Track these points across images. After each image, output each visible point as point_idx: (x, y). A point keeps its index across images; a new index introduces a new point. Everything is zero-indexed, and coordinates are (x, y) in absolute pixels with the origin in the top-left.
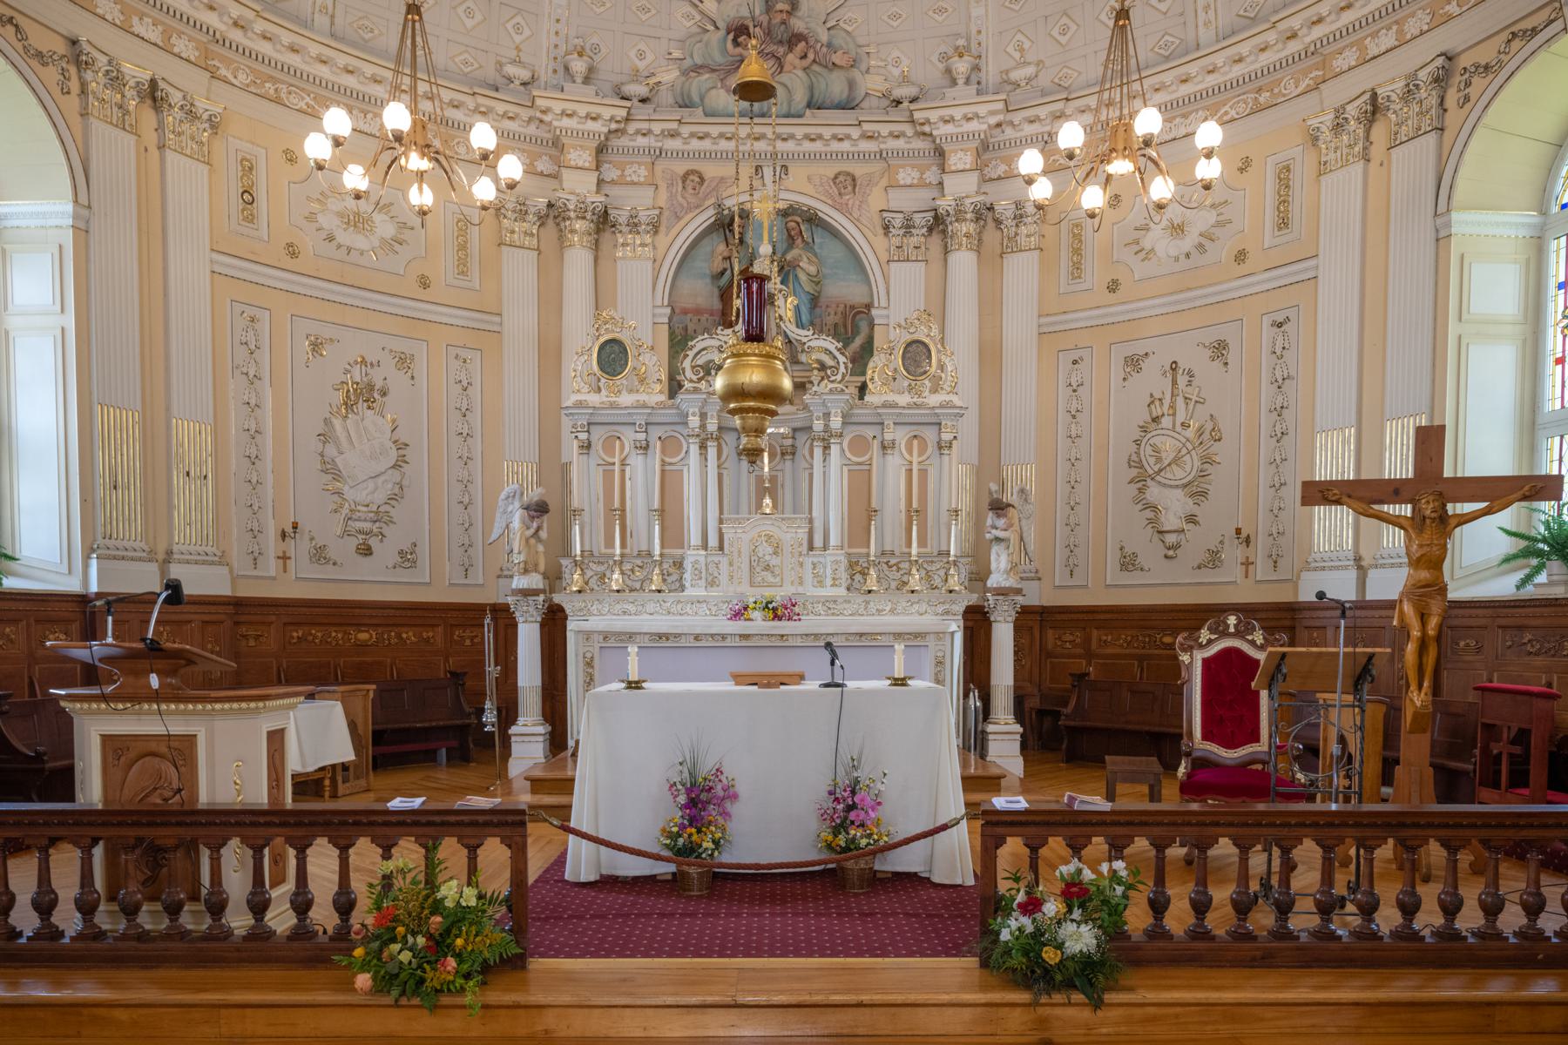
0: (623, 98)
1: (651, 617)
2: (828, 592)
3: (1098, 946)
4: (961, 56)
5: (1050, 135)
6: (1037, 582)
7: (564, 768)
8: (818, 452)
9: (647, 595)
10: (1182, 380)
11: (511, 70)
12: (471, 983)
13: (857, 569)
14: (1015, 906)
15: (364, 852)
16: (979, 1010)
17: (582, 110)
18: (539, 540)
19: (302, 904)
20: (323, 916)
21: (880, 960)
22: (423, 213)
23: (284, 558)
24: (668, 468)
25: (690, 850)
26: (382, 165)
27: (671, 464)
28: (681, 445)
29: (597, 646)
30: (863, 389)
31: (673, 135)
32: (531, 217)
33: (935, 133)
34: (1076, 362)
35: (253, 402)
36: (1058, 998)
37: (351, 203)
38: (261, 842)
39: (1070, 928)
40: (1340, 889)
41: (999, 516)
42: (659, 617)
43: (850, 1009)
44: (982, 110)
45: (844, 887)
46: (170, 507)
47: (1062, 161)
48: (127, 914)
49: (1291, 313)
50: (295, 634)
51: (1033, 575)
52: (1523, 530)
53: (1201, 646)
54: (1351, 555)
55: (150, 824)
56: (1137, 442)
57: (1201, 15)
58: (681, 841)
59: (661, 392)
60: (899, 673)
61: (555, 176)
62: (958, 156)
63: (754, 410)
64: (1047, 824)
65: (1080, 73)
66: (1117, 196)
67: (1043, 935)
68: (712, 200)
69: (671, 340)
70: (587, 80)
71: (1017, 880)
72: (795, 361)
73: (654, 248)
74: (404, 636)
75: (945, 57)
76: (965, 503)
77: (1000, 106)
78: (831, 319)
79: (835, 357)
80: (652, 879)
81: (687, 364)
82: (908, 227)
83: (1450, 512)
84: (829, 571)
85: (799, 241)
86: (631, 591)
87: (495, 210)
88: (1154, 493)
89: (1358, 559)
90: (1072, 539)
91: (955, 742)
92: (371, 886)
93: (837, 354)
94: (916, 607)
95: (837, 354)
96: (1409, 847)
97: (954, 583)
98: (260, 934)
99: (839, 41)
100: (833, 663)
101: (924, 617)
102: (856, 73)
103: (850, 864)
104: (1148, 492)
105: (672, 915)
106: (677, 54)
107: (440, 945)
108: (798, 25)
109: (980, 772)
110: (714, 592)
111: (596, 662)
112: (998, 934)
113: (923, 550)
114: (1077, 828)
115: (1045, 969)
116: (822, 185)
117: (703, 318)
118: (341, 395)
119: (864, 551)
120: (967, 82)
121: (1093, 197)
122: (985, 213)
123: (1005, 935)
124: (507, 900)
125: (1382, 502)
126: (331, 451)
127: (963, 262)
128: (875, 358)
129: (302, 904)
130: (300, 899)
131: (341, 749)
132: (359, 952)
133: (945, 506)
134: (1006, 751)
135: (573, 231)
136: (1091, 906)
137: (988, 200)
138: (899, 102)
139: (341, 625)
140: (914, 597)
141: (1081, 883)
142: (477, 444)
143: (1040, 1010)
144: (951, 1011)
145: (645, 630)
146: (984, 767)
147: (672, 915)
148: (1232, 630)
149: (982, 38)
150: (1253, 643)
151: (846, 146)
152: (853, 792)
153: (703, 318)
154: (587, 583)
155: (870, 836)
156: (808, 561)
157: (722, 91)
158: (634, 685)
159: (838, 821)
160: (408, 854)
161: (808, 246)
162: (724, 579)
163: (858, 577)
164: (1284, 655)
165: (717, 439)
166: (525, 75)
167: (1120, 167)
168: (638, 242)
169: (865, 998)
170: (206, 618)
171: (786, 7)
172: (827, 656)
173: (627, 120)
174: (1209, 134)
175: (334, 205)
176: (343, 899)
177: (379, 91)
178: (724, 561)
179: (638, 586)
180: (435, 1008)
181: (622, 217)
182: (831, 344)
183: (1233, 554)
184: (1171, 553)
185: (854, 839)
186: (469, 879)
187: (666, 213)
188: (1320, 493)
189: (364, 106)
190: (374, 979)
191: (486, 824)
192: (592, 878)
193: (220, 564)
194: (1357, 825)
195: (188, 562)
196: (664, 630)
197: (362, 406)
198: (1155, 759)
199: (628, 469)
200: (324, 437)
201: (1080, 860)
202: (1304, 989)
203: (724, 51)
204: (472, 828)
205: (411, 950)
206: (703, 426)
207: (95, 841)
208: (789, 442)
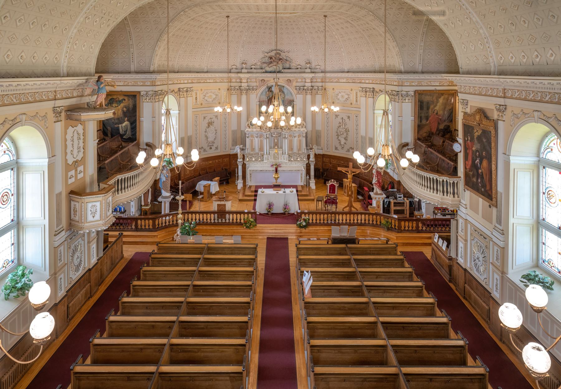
2: (286, 161)
9: (258, 162)
10: (344, 121)
25: (269, 212)
107: (251, 225)
108: (281, 57)
135: (243, 93)
162: (270, 159)
178: (270, 156)
200: (205, 132)
203: (268, 60)
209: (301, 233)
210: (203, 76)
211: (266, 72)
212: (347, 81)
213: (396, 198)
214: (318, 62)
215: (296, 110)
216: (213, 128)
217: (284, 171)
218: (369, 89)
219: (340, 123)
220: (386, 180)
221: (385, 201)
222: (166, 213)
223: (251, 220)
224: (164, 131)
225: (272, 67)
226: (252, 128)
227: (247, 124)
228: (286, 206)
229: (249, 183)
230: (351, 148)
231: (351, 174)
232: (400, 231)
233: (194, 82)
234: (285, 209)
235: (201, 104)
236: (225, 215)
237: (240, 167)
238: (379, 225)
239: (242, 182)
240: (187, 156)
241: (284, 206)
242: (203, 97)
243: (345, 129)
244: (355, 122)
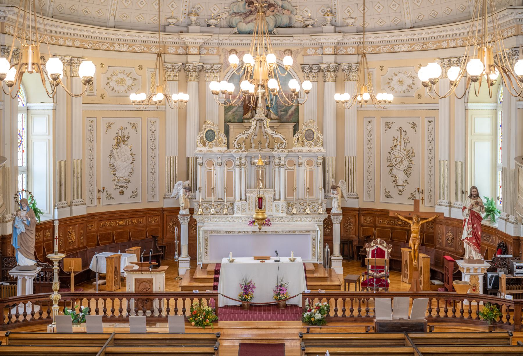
2: (280, 214)
6: (357, 200)
10: (403, 134)
13: (289, 205)
23: (99, 199)
25: (245, 300)
27: (229, 170)
29: (209, 235)
39: (317, 314)
42: (226, 223)
50: (102, 224)
51: (356, 196)
53: (371, 247)
57: (406, 15)
58: (243, 298)
62: (328, 49)
65: (369, 24)
74: (133, 221)
84: (280, 208)
90: (369, 185)
94: (308, 219)
103: (280, 303)
107: (205, 318)
123: (305, 316)
135: (192, 76)
139: (114, 219)
148: (379, 243)
149: (336, 6)
150: (384, 246)
152: (281, 287)
156: (274, 204)
157: (244, 23)
160: (196, 301)
162: (247, 209)
163: (290, 208)
168: (213, 76)
170: (80, 222)
178: (247, 204)
179: (219, 211)
184: (400, 193)
192: (223, 306)
196: (229, 230)
197: (121, 144)
200: (111, 156)
203: (244, 8)
210: (106, 36)
211: (240, 33)
212: (410, 49)
213: (511, 272)
214: (349, 11)
215: (304, 115)
216: (128, 149)
217: (276, 232)
218: (456, 59)
219: (395, 139)
220: (490, 246)
221: (489, 275)
222: (27, 293)
223: (206, 308)
224: (24, 146)
225: (251, 21)
226: (209, 145)
227: (198, 138)
228: (280, 289)
229: (201, 260)
230: (418, 189)
231: (418, 222)
232: (517, 327)
233: (86, 45)
234: (278, 294)
235: (102, 96)
236: (152, 301)
237: (184, 228)
238: (476, 319)
239: (189, 259)
240: (71, 203)
241: (276, 289)
242: (107, 81)
243: (405, 152)
244: (427, 133)
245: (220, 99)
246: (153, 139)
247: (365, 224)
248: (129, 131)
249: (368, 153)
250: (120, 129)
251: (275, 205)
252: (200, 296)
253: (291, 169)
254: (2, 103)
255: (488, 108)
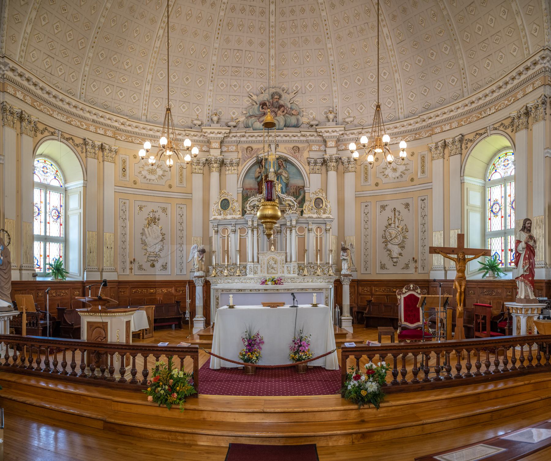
0: (228, 126)
1: (236, 284)
2: (292, 275)
3: (378, 389)
4: (331, 113)
5: (358, 138)
6: (356, 272)
7: (209, 331)
8: (288, 232)
9: (235, 277)
10: (397, 214)
11: (195, 122)
12: (181, 402)
13: (301, 268)
14: (352, 378)
15: (151, 358)
16: (341, 412)
17: (216, 131)
18: (203, 261)
19: (134, 373)
20: (140, 377)
21: (310, 396)
22: (170, 167)
23: (131, 269)
24: (242, 237)
25: (248, 360)
26: (159, 155)
27: (242, 236)
28: (246, 230)
29: (220, 293)
30: (302, 212)
31: (243, 136)
32: (201, 164)
33: (323, 135)
34: (366, 206)
35: (124, 226)
36: (366, 406)
37: (151, 167)
38: (123, 354)
39: (369, 384)
40: (442, 364)
41: (344, 252)
43: (300, 414)
44: (338, 129)
45: (298, 371)
46: (103, 257)
47: (361, 146)
48: (92, 371)
49: (426, 197)
52: (483, 262)
53: (403, 294)
54: (443, 267)
55: (98, 347)
56: (385, 231)
58: (246, 357)
59: (240, 214)
60: (315, 303)
61: (208, 151)
63: (269, 222)
64: (362, 351)
66: (377, 158)
67: (361, 386)
68: (255, 155)
69: (243, 198)
70: (218, 122)
71: (353, 369)
72: (281, 203)
73: (238, 170)
75: (326, 113)
76: (334, 248)
77: (343, 129)
78: (292, 191)
79: (293, 203)
80: (237, 369)
81: (248, 205)
82: (316, 163)
83: (466, 258)
84: (292, 269)
85: (282, 167)
86: (230, 276)
87: (191, 163)
88: (390, 246)
89: (445, 268)
91: (332, 322)
92: (153, 369)
93: (294, 202)
94: (319, 280)
95: (294, 202)
96: (458, 352)
97: (331, 272)
98: (122, 381)
99: (294, 107)
100: (294, 300)
101: (322, 283)
102: (299, 117)
104: (388, 246)
105: (243, 381)
106: (245, 112)
107: (172, 389)
108: (281, 102)
109: (340, 332)
110: (256, 276)
111: (219, 299)
112: (347, 387)
113: (321, 262)
114: (370, 351)
115: (362, 397)
116: (289, 150)
117: (252, 191)
118: (147, 222)
119: (303, 262)
120: (333, 121)
121: (371, 158)
122: (339, 160)
123: (349, 387)
124: (192, 375)
125: (450, 254)
126: (144, 237)
127: (332, 174)
128: (306, 203)
129: (134, 373)
130: (133, 371)
131: (145, 325)
132: (149, 389)
133: (328, 249)
134: (347, 326)
135: (213, 167)
136: (375, 376)
137: (340, 156)
138: (312, 126)
140: (319, 277)
141: (372, 369)
142: (184, 233)
143: (361, 411)
144: (333, 413)
145: (235, 288)
146: (341, 331)
147: (243, 381)
148: (412, 289)
149: (337, 108)
150: (417, 292)
151: (296, 138)
152: (301, 341)
153: (252, 191)
154: (217, 274)
155: (306, 355)
156: (285, 266)
158: (231, 307)
159: (296, 350)
160: (163, 359)
161: (285, 168)
162: (259, 271)
164: (425, 297)
165: (257, 228)
166: (199, 123)
167: (378, 150)
168: (233, 169)
169: (305, 409)
171: (278, 97)
172: (292, 297)
173: (229, 133)
174: (403, 144)
175: (146, 168)
176: (145, 372)
177: (159, 134)
178: (259, 266)
179: (232, 274)
180: (171, 408)
181: (228, 162)
182: (292, 199)
183: (412, 265)
184: (395, 264)
185: (301, 356)
186: (181, 368)
187: (241, 160)
188: (434, 250)
189: (154, 139)
190: (153, 398)
191: (186, 351)
192: (218, 368)
193: (115, 272)
194: (445, 347)
195: (107, 272)
197: (152, 224)
198: (392, 327)
199: (229, 238)
200: (142, 234)
201: (372, 362)
202: (432, 397)
203: (259, 110)
204: (182, 352)
205: (164, 390)
206: (253, 224)
207: (85, 350)
208: (279, 229)
209: (363, 422)
226: (224, 214)
245: (239, 189)
246: (181, 221)
247: (363, 293)
248: (160, 214)
249: (365, 232)
250: (151, 212)
251: (287, 267)
252: (170, 351)
253: (301, 235)
254: (2, 157)
255: (478, 184)
